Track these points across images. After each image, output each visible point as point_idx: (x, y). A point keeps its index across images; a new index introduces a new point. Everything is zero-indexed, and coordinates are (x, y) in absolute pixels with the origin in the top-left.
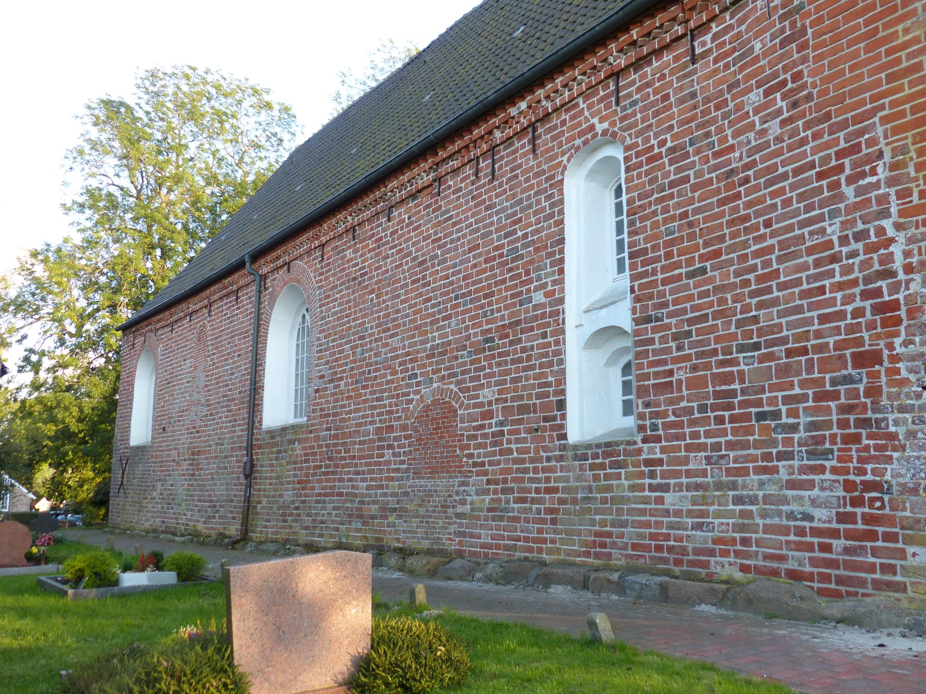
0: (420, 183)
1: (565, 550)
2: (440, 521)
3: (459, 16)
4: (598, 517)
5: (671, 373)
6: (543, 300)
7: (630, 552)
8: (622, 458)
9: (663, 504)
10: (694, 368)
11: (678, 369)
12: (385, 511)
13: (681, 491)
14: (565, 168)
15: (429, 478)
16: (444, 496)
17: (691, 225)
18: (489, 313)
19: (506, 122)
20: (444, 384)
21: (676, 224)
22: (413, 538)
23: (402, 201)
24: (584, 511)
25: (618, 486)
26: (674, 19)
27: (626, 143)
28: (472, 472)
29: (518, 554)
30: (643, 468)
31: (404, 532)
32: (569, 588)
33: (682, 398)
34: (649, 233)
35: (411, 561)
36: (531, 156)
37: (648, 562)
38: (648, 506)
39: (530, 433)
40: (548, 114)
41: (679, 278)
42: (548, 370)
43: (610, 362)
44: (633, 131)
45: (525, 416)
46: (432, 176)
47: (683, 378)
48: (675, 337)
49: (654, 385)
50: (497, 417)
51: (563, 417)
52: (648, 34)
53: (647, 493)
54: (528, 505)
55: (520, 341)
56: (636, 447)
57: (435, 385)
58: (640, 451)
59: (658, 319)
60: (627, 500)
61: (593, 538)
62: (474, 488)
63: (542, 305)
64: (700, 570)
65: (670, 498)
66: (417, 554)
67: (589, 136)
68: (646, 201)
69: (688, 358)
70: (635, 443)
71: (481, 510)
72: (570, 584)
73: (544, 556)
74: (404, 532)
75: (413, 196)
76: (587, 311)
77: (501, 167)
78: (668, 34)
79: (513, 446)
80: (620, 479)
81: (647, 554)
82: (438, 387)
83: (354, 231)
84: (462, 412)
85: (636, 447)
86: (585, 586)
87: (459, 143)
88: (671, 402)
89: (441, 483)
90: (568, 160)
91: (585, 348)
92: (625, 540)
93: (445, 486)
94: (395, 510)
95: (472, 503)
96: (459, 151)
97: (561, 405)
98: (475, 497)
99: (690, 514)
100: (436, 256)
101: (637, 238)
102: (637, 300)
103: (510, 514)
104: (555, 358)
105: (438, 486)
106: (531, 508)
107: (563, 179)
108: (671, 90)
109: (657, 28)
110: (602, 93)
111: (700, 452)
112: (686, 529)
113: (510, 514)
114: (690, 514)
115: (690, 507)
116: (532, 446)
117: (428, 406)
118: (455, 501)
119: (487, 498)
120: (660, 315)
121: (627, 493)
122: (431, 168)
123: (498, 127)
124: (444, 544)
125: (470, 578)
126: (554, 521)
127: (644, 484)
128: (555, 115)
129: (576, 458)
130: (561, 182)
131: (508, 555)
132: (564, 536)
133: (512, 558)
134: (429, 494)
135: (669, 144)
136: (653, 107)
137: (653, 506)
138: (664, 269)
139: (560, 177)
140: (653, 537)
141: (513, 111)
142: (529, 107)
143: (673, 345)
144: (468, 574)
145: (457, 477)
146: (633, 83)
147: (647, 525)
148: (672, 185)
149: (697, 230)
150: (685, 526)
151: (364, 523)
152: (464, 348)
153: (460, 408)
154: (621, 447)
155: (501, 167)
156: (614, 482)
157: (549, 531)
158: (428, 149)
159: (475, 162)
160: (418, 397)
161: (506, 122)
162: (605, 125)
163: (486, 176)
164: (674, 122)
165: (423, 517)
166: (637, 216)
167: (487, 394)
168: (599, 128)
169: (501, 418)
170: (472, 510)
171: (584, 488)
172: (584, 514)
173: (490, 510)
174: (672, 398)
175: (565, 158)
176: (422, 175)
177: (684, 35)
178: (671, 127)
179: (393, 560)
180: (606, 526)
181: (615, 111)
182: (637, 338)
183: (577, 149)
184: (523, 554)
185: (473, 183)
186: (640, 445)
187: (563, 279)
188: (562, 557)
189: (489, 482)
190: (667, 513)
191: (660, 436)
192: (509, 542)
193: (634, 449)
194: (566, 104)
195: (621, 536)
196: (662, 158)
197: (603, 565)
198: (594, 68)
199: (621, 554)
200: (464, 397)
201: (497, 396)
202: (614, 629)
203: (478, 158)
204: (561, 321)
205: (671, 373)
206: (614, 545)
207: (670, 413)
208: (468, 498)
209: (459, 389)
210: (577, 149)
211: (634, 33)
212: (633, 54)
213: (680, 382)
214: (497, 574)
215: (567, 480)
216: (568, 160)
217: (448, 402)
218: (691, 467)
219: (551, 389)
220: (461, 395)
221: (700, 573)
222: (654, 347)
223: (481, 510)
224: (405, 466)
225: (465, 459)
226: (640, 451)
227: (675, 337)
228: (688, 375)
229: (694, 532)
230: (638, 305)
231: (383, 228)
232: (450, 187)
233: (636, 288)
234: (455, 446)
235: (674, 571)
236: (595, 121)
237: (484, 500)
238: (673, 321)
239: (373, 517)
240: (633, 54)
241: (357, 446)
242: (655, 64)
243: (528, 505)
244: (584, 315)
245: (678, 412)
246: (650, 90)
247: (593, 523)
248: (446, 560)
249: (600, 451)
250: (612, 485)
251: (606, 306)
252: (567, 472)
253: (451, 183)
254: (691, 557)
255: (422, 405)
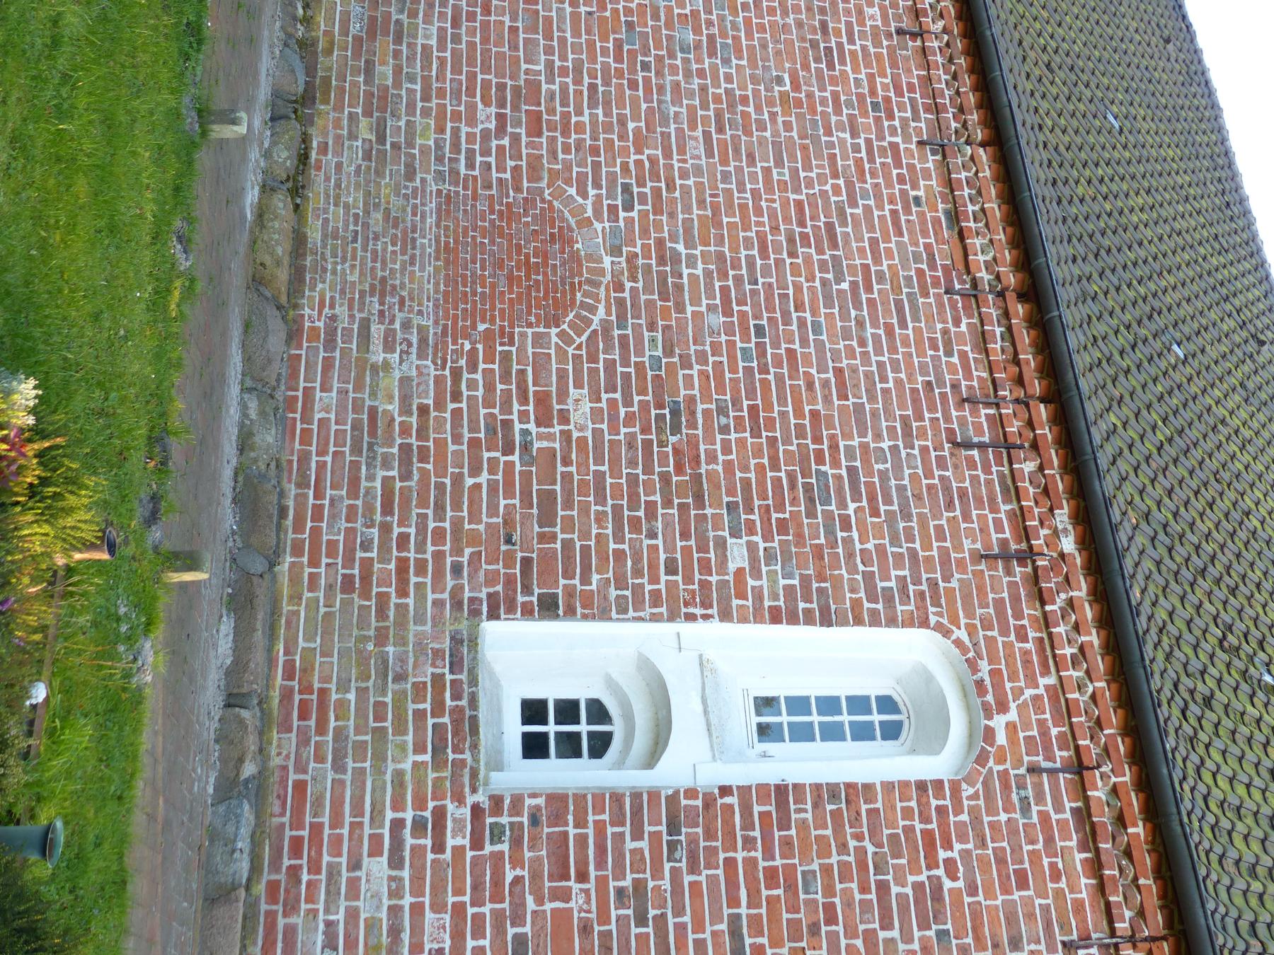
0: (976, 242)
1: (297, 613)
2: (354, 277)
3: (1223, 98)
4: (351, 696)
5: (582, 877)
6: (732, 567)
7: (292, 777)
8: (451, 756)
9: (369, 856)
10: (586, 929)
11: (587, 892)
12: (379, 103)
13: (390, 896)
14: (946, 633)
15: (438, 241)
16: (403, 286)
17: (814, 930)
18: (723, 420)
19: (1046, 491)
20: (607, 289)
21: (819, 896)
22: (328, 196)
23: (950, 184)
24: (363, 659)
25: (402, 748)
26: (1141, 913)
27: (964, 786)
28: (444, 368)
29: (292, 490)
30: (431, 805)
31: (339, 166)
32: (228, 662)
33: (540, 901)
34: (814, 833)
35: (281, 203)
36: (978, 546)
37: (276, 820)
38: (367, 820)
39: (505, 522)
40: (1043, 603)
41: (734, 901)
42: (611, 575)
43: (611, 684)
44: (981, 802)
45: (535, 511)
46: (984, 275)
47: (572, 904)
48: (639, 886)
49: (566, 834)
50: (540, 437)
51: (528, 612)
52: (1128, 854)
53: (389, 815)
54: (378, 517)
55: (668, 503)
56: (467, 790)
57: (607, 261)
58: (460, 800)
59: (672, 846)
60: (379, 771)
61: (316, 685)
62: (414, 373)
63: (723, 561)
64: (260, 943)
65: (377, 868)
66: (297, 207)
67: (990, 698)
68: (865, 830)
69: (604, 917)
70: (474, 790)
71: (373, 395)
72: (236, 662)
73: (289, 559)
74: (339, 166)
75: (955, 216)
76: (701, 656)
77: (972, 464)
78: (1121, 899)
79: (484, 478)
80: (415, 752)
81: (286, 819)
82: (602, 272)
83: (914, 36)
84: (555, 339)
85: (467, 790)
86: (233, 700)
87: (1028, 357)
88: (536, 876)
89: (426, 277)
90: (958, 643)
91: (640, 654)
92: (312, 765)
93: (421, 289)
94: (381, 139)
95: (386, 365)
96: (1016, 361)
97: (548, 608)
98: (397, 374)
99: (352, 915)
100: (839, 280)
101: (809, 807)
102: (709, 801)
103: (364, 468)
104: (634, 605)
105: (422, 269)
106: (372, 526)
107: (928, 627)
108: (1031, 893)
109: (1136, 879)
110: (1054, 731)
111: (452, 938)
112: (327, 911)
113: (364, 468)
114: (352, 915)
115: (363, 916)
116: (481, 527)
117: (571, 242)
118: (392, 322)
119: (394, 408)
120: (677, 855)
121: (391, 767)
122: (998, 277)
123: (1041, 468)
124: (313, 289)
125: (249, 383)
126: (348, 583)
127: (404, 810)
128: (1038, 613)
129: (456, 640)
130: (924, 624)
131: (291, 462)
132: (322, 610)
133: (286, 474)
134: (408, 242)
135: (948, 884)
136: (1013, 851)
137: (367, 831)
138: (751, 863)
139: (933, 620)
140: (316, 829)
141: (1062, 517)
142: (1062, 556)
143: (627, 883)
144: (256, 384)
145: (436, 323)
146: (1059, 808)
147: (336, 822)
148: (883, 888)
149: (804, 944)
150: (333, 909)
151: (358, 39)
152: (668, 352)
153: (562, 335)
154: (467, 756)
155: (972, 464)
156: (410, 738)
157: (332, 572)
158: (1034, 290)
159: (992, 400)
160: (590, 213)
161: (1046, 491)
162: (1001, 739)
163: (962, 422)
164: (981, 898)
165: (366, 226)
166: (843, 806)
167: (580, 406)
168: (999, 722)
169: (537, 445)
170: (375, 369)
171: (402, 660)
172: (358, 664)
173: (373, 412)
174: (542, 877)
175: (962, 634)
176: (990, 252)
177: (1113, 933)
178: (973, 891)
179: (285, 154)
180: (337, 719)
181: (1018, 763)
182: (645, 797)
183: (973, 666)
184: (291, 504)
185: (955, 386)
186: (470, 800)
187: (762, 621)
188: (286, 608)
189: (423, 410)
190: (355, 865)
191: (482, 848)
192: (313, 465)
193: (463, 786)
194: (1053, 648)
195: (320, 759)
196: (929, 868)
197: (270, 709)
198: (1099, 723)
199: (288, 756)
200: (579, 347)
201: (575, 435)
202: (222, 142)
203: (997, 405)
204: (691, 610)
205: (582, 877)
206: (304, 741)
207: (518, 872)
208: (397, 355)
209: (595, 331)
210: (973, 666)
211: (1138, 830)
212: (1103, 818)
213: (565, 895)
214: (255, 460)
215: (420, 619)
216: (958, 643)
217: (573, 300)
218: (429, 915)
219: (577, 582)
220: (584, 338)
221: (255, 943)
222: (628, 837)
223: (373, 395)
224: (463, 171)
225: (467, 347)
226: (459, 799)
227: (639, 886)
228: (576, 914)
229: (321, 926)
230: (699, 803)
231: (909, 125)
232: (957, 322)
233: (728, 800)
234: (492, 321)
235: (258, 882)
236: (1013, 715)
237: (390, 398)
238: (666, 884)
239: (369, 70)
240: (1103, 818)
241: (507, 19)
242: (1079, 857)
243: (378, 517)
244: (696, 654)
245: (518, 889)
246: (1040, 846)
247: (343, 687)
248: (283, 300)
249: (464, 703)
250: (405, 733)
251: (706, 712)
252: (433, 618)
253: (963, 328)
254: (281, 922)
255: (572, 222)
